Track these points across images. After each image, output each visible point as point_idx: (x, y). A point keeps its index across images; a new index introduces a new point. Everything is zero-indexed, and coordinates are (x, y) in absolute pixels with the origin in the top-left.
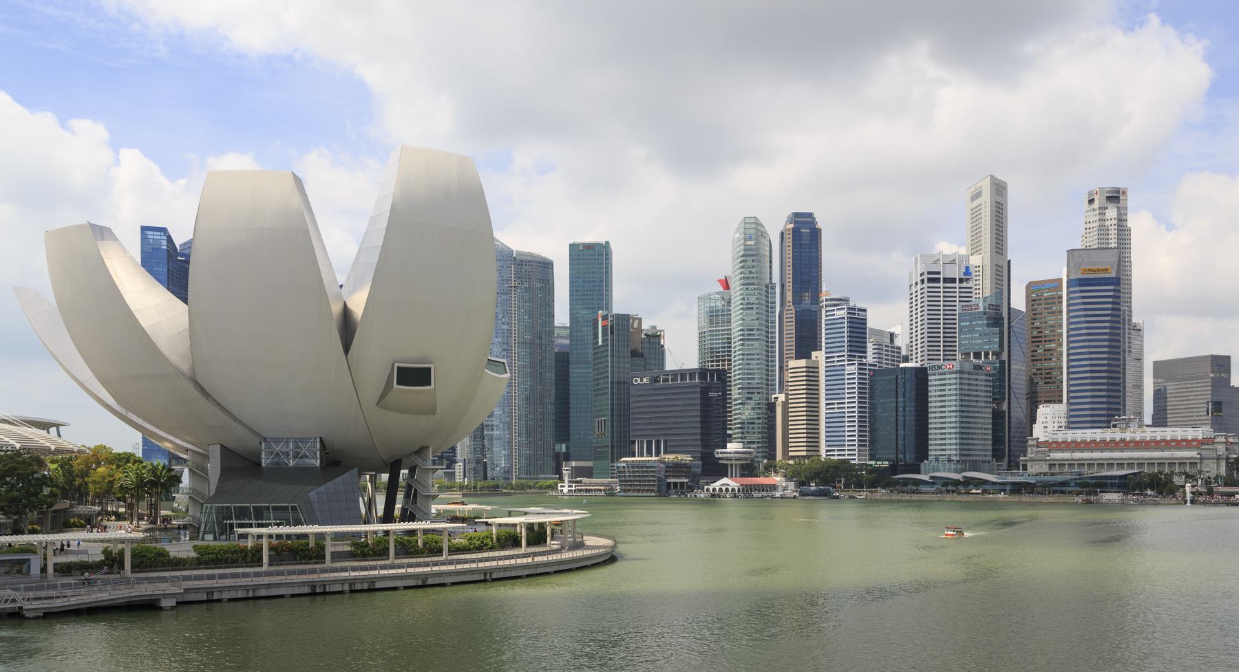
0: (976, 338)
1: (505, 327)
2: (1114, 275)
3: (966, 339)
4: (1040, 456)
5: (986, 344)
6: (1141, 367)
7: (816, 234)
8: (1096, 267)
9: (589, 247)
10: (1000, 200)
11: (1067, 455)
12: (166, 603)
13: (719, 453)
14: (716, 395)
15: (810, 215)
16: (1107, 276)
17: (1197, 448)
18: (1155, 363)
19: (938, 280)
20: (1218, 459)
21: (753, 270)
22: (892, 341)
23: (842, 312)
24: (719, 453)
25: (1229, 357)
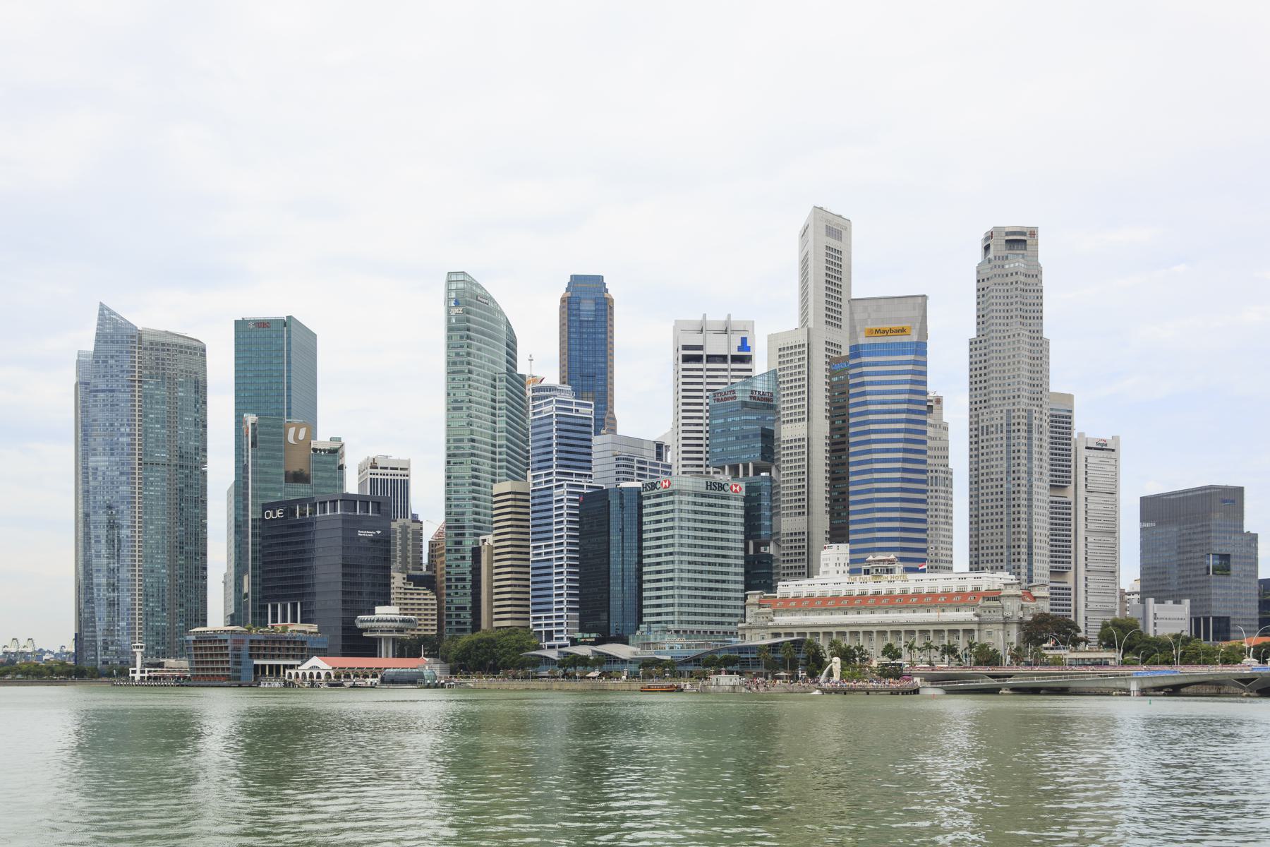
0: (732, 444)
1: (124, 440)
2: (915, 338)
3: (718, 445)
4: (761, 621)
5: (744, 451)
6: (1115, 504)
7: (604, 307)
8: (886, 327)
9: (262, 324)
10: (834, 243)
11: (933, 616)
12: (1112, 662)
13: (363, 621)
14: (370, 534)
15: (599, 280)
16: (905, 339)
17: (972, 607)
18: (1144, 500)
19: (698, 359)
20: (1006, 622)
21: (462, 352)
22: (659, 455)
23: (549, 407)
24: (363, 621)
25: (1240, 490)
